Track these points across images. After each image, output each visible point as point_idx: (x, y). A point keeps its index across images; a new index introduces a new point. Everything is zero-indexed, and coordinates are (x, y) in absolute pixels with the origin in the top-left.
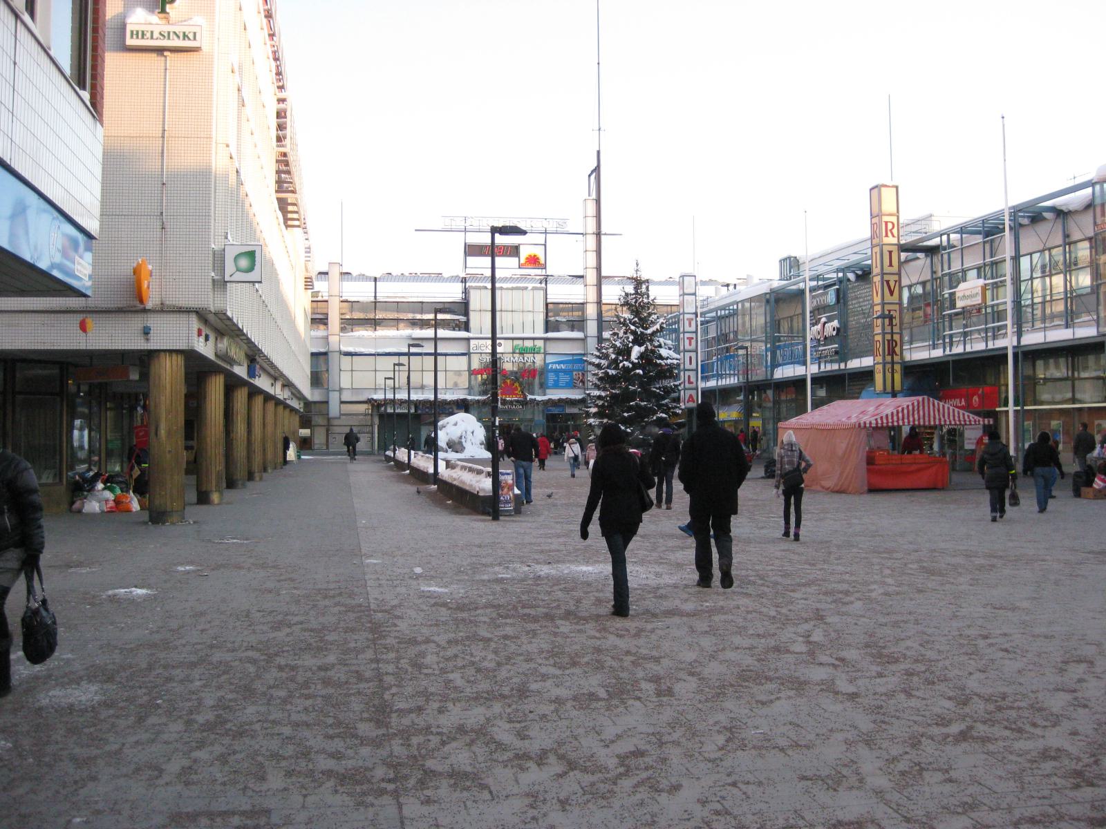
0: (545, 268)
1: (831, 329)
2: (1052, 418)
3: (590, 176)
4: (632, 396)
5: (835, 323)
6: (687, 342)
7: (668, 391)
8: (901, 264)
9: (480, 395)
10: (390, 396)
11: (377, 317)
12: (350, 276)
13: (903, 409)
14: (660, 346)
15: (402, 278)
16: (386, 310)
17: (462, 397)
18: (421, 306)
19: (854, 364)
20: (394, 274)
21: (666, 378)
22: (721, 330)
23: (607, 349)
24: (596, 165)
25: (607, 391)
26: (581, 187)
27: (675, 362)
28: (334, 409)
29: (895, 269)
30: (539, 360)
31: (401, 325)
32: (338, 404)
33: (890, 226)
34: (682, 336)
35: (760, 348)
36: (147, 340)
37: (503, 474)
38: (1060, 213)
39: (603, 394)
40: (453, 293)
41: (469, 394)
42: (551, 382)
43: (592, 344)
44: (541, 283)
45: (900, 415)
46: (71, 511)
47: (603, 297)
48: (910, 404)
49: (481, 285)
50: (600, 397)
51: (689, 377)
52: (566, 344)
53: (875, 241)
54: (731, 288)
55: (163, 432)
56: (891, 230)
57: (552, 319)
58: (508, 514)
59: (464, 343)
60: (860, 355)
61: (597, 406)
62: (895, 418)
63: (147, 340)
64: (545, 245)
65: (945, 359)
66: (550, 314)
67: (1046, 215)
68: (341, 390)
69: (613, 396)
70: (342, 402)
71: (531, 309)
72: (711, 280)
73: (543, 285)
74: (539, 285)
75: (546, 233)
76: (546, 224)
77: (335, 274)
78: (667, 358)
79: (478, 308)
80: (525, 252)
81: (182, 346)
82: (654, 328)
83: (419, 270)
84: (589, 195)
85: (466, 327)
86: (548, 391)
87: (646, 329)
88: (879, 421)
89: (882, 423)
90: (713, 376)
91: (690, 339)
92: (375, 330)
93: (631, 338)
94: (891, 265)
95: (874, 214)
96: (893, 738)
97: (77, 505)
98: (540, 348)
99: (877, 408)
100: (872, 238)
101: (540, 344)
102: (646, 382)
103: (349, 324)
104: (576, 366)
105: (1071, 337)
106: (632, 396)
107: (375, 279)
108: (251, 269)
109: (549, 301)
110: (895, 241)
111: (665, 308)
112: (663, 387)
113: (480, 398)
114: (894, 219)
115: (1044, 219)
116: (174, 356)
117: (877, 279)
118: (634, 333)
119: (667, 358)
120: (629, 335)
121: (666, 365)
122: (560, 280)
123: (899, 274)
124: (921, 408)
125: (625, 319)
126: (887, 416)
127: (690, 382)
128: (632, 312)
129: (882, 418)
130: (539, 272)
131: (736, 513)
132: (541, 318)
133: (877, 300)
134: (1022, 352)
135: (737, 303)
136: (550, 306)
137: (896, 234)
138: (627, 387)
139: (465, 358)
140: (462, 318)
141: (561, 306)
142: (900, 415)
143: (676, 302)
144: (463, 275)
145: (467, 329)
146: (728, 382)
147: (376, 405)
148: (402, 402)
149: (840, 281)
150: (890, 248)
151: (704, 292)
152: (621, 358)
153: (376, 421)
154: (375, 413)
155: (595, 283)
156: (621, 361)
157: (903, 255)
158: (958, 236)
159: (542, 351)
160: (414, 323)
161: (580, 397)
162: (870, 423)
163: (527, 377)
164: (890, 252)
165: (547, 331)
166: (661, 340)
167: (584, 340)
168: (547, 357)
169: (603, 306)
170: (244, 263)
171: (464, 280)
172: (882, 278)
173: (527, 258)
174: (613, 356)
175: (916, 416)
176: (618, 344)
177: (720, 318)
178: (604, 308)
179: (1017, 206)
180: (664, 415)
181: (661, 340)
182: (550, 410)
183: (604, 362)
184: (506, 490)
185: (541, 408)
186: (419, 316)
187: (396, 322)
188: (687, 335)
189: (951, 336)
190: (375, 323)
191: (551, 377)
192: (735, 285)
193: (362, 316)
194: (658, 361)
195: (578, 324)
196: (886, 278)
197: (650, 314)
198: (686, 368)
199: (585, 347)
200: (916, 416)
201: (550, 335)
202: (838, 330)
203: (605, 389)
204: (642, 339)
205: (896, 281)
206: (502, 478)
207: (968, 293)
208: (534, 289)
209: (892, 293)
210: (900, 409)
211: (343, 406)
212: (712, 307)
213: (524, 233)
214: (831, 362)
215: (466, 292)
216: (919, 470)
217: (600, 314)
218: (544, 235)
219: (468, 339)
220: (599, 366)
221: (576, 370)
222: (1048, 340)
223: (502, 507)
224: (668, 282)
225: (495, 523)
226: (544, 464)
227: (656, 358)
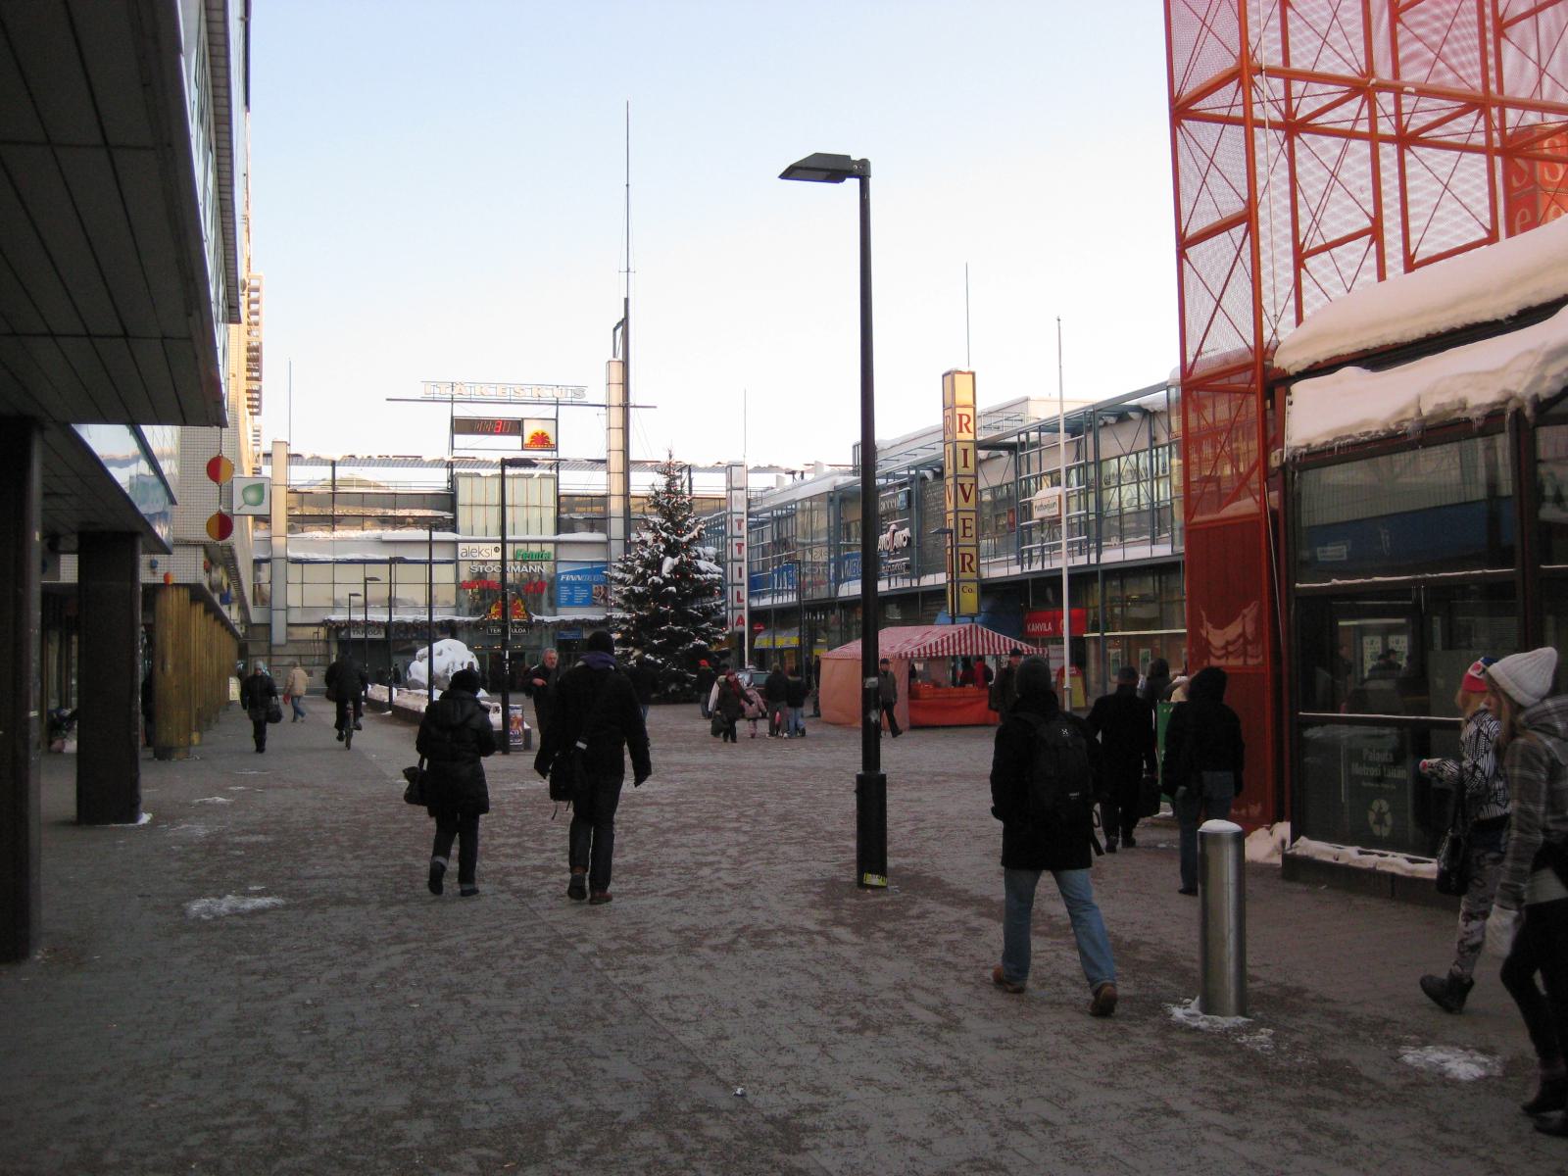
0: (557, 450)
1: (901, 539)
3: (615, 330)
4: (663, 618)
5: (906, 532)
6: (736, 549)
7: (708, 614)
8: (979, 462)
9: (470, 615)
10: (359, 617)
11: (336, 513)
12: (300, 459)
13: (948, 638)
14: (698, 557)
15: (369, 461)
16: (347, 504)
17: (448, 618)
18: (395, 499)
19: (929, 581)
20: (359, 457)
21: (705, 595)
22: (778, 534)
23: (633, 561)
24: (623, 316)
25: (634, 612)
26: (604, 347)
27: (716, 576)
28: (279, 635)
29: (971, 470)
30: (546, 568)
31: (368, 524)
32: (284, 626)
34: (729, 541)
35: (821, 555)
36: (154, 573)
37: (513, 708)
38: (1147, 414)
39: (628, 616)
40: (435, 480)
41: (457, 615)
42: (563, 599)
43: (617, 549)
44: (551, 469)
45: (945, 644)
46: (50, 751)
47: (631, 488)
48: (956, 632)
49: (474, 471)
50: (623, 621)
52: (583, 548)
53: (949, 437)
54: (798, 476)
55: (169, 667)
56: (969, 565)
57: (565, 516)
58: (517, 749)
59: (450, 548)
60: (935, 571)
61: (620, 631)
62: (940, 648)
63: (154, 573)
64: (556, 420)
65: (1025, 578)
66: (562, 510)
67: (1133, 415)
68: (287, 608)
69: (640, 619)
70: (290, 625)
71: (538, 504)
72: (771, 467)
73: (554, 472)
74: (548, 472)
75: (557, 404)
76: (557, 393)
77: (280, 456)
78: (707, 572)
79: (468, 501)
80: (530, 429)
81: (190, 580)
82: (691, 535)
83: (392, 452)
84: (614, 356)
85: (453, 525)
86: (560, 610)
87: (682, 536)
88: (922, 652)
89: (925, 654)
90: (769, 592)
92: (334, 530)
93: (662, 547)
94: (966, 466)
95: (947, 406)
97: (56, 745)
98: (549, 553)
99: (923, 637)
100: (945, 429)
101: (549, 548)
102: (680, 601)
103: (298, 522)
104: (596, 578)
105: (1121, 559)
106: (663, 618)
107: (333, 464)
108: (259, 502)
109: (561, 492)
110: (970, 437)
111: (712, 503)
112: (702, 608)
113: (471, 619)
114: (969, 412)
115: (1131, 419)
116: (181, 590)
117: (950, 482)
118: (666, 541)
119: (707, 572)
120: (659, 543)
121: (706, 580)
122: (577, 465)
123: (976, 477)
124: (968, 637)
125: (655, 524)
126: (931, 646)
128: (664, 515)
129: (925, 648)
130: (547, 454)
132: (550, 514)
133: (950, 506)
135: (796, 502)
136: (563, 499)
137: (972, 429)
138: (657, 608)
139: (451, 567)
140: (448, 515)
141: (577, 499)
142: (945, 644)
143: (723, 494)
144: (448, 458)
145: (455, 530)
146: (785, 601)
147: (333, 628)
148: (378, 625)
149: (912, 478)
150: (965, 446)
151: (758, 483)
152: (650, 572)
153: (334, 649)
154: (332, 639)
155: (621, 470)
156: (650, 576)
157: (983, 454)
158: (1037, 434)
159: (552, 557)
160: (385, 521)
161: (602, 618)
162: (912, 653)
163: (537, 590)
164: (965, 451)
165: (558, 531)
166: (700, 549)
167: (606, 543)
168: (559, 565)
169: (632, 500)
170: (252, 496)
171: (450, 465)
173: (533, 437)
174: (640, 570)
175: (963, 646)
176: (646, 554)
177: (778, 519)
178: (633, 501)
179: (1097, 404)
180: (703, 643)
181: (700, 549)
182: (562, 635)
183: (629, 577)
184: (515, 725)
185: (550, 631)
186: (390, 512)
187: (360, 520)
189: (1030, 551)
190: (333, 521)
191: (564, 592)
192: (802, 473)
193: (315, 511)
194: (696, 576)
195: (599, 523)
196: (960, 480)
197: (686, 518)
199: (608, 551)
200: (963, 646)
201: (563, 537)
202: (910, 540)
203: (629, 611)
204: (676, 548)
206: (511, 712)
207: (1045, 503)
208: (542, 476)
209: (967, 499)
210: (945, 638)
211: (293, 630)
212: (766, 506)
213: (535, 465)
214: (903, 577)
215: (452, 479)
216: (971, 704)
217: (627, 510)
218: (555, 407)
219: (455, 543)
220: (622, 582)
221: (597, 583)
222: (1126, 559)
223: (513, 743)
224: (713, 469)
225: (506, 757)
227: (693, 571)
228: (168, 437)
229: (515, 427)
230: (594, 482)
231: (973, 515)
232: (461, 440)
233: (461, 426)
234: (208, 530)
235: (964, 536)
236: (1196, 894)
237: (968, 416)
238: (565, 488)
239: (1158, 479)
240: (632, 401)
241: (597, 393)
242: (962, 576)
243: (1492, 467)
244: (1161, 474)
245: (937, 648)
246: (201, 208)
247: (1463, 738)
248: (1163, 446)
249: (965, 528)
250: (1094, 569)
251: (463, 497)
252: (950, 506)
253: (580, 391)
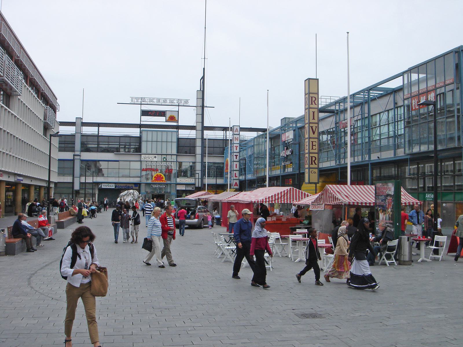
51: (235, 174)
56: (314, 161)
80: (168, 115)
91: (236, 156)
94: (314, 119)
123: (318, 124)
127: (236, 176)
134: (370, 163)
137: (317, 104)
150: (314, 110)
172: (309, 125)
188: (235, 154)
196: (311, 125)
198: (234, 160)
205: (316, 127)
229: (162, 114)
230: (191, 134)
231: (316, 140)
232: (144, 118)
233: (145, 113)
237: (315, 158)
238: (180, 136)
239: (398, 122)
240: (205, 105)
241: (193, 101)
243: (420, 181)
244: (399, 119)
245: (272, 198)
246: (405, 191)
248: (400, 107)
249: (313, 145)
250: (368, 162)
251: (144, 138)
252: (307, 136)
253: (187, 101)
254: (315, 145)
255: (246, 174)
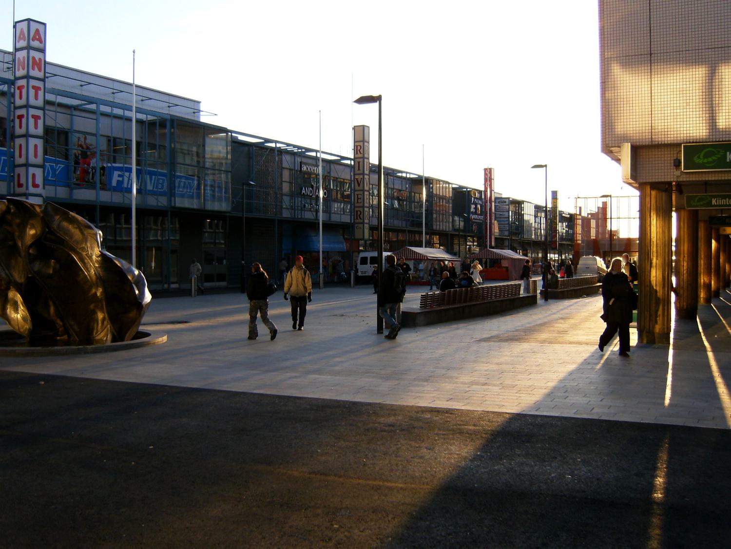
2: (555, 230)
33: (359, 213)
51: (34, 175)
56: (359, 150)
94: (359, 169)
96: (377, 543)
131: (402, 302)
209: (359, 186)
226: (303, 313)
228: (415, 307)
234: (600, 338)
235: (358, 202)
236: (111, 342)
237: (360, 212)
242: (357, 205)
247: (598, 258)
249: (358, 198)
254: (360, 199)
255: (590, 327)
